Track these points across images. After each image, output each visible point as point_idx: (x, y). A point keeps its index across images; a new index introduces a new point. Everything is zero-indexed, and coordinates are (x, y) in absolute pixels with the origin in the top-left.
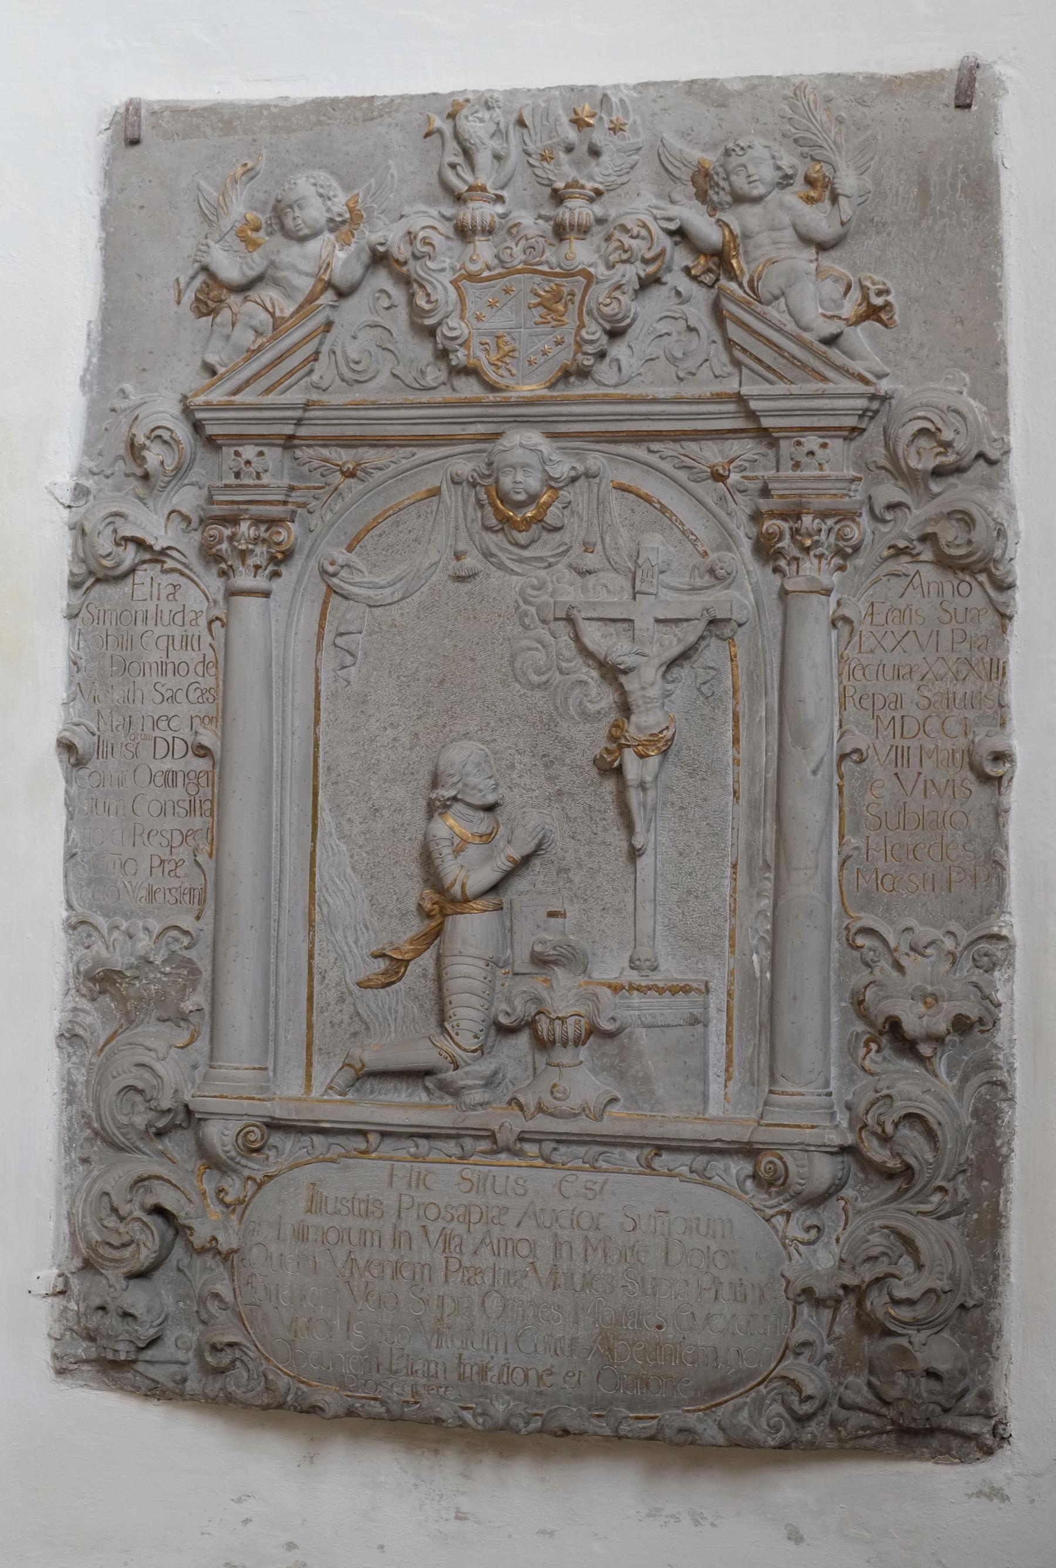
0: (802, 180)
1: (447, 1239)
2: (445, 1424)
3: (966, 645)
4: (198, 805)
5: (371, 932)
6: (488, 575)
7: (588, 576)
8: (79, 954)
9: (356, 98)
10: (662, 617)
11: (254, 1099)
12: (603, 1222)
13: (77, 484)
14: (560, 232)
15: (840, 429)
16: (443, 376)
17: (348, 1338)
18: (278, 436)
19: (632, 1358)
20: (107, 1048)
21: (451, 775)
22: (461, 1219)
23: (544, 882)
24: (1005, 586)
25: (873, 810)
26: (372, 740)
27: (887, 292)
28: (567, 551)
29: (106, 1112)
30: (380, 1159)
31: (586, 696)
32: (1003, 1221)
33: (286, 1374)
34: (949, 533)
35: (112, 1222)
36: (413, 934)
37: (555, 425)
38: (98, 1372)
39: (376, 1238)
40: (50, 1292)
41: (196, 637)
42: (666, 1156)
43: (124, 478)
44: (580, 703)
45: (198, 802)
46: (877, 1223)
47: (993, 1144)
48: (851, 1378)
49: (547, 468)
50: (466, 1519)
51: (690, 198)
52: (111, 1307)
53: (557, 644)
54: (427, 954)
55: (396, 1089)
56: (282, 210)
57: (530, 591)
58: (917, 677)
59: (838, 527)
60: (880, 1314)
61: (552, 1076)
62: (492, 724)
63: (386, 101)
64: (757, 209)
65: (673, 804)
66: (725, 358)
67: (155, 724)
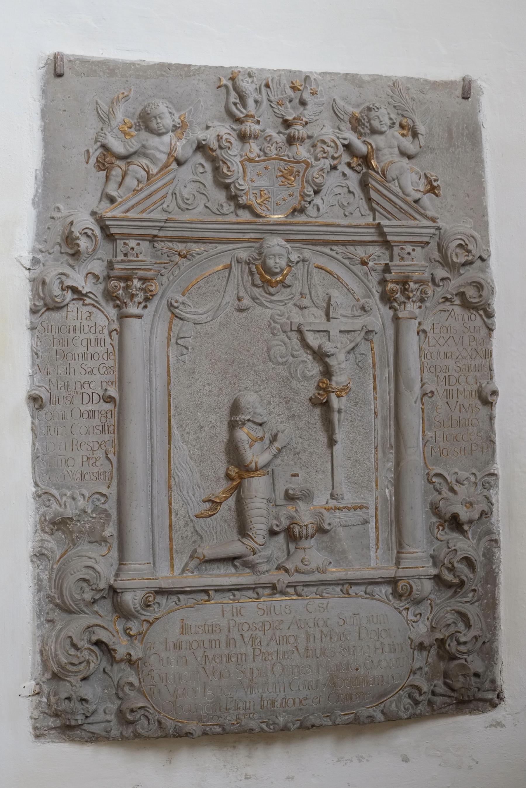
0: (398, 125)
1: (253, 639)
2: (254, 732)
3: (475, 343)
4: (106, 428)
5: (201, 489)
6: (254, 309)
7: (305, 310)
8: (43, 510)
9: (181, 65)
10: (343, 330)
11: (150, 579)
12: (329, 622)
13: (34, 257)
14: (291, 141)
15: (421, 242)
16: (232, 208)
17: (205, 696)
18: (149, 235)
19: (345, 686)
20: (62, 559)
21: (248, 408)
22: (260, 629)
23: (287, 460)
24: (490, 315)
25: (437, 419)
26: (198, 392)
27: (438, 180)
28: (293, 297)
29: (66, 593)
30: (216, 603)
31: (306, 368)
32: (497, 602)
33: (170, 719)
34: (471, 292)
35: (73, 652)
36: (223, 489)
37: (289, 235)
38: (59, 733)
39: (218, 643)
40: (32, 693)
41: (103, 340)
42: (354, 588)
43: (60, 255)
44: (303, 372)
45: (106, 426)
46: (448, 609)
47: (492, 567)
48: (436, 682)
49: (289, 256)
50: (250, 778)
51: (348, 129)
52: (74, 697)
53: (291, 343)
54: (230, 499)
55: (218, 567)
56: (150, 118)
57: (276, 317)
58: (454, 357)
59: (421, 288)
60: (454, 650)
61: (300, 554)
62: (259, 383)
63: (196, 68)
64: (382, 137)
65: (347, 419)
66: (366, 207)
67: (82, 386)
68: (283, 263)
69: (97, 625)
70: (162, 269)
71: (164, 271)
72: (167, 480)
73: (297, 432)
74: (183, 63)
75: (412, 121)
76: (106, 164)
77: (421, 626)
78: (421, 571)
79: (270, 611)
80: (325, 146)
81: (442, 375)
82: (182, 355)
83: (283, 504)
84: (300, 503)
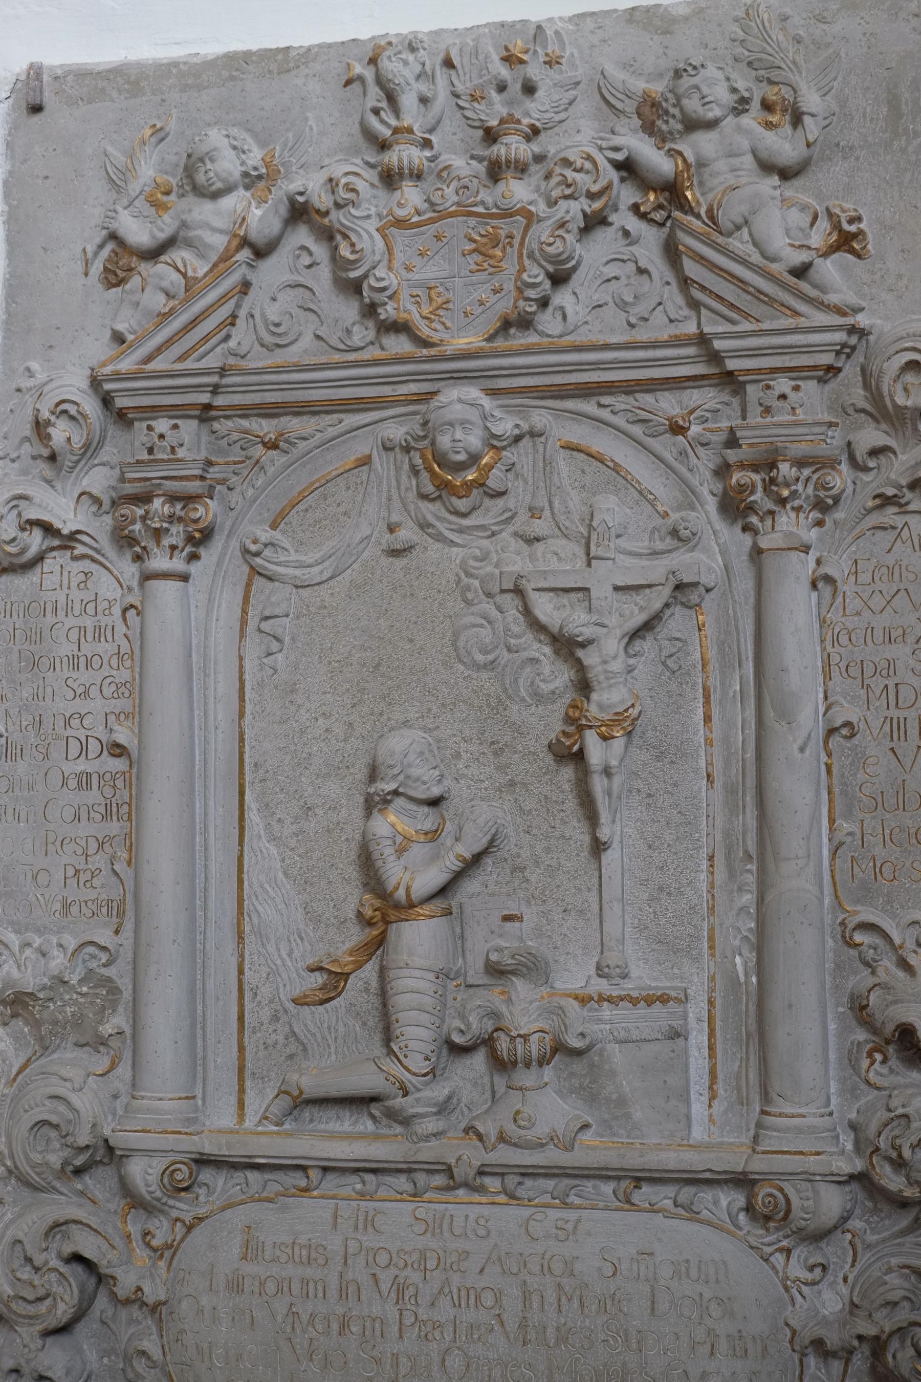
0: (759, 106)
1: (400, 1290)
4: (114, 809)
5: (306, 943)
6: (426, 548)
7: (537, 544)
9: (271, 50)
11: (179, 1133)
12: (578, 1267)
15: (815, 368)
16: (371, 334)
20: (20, 1077)
21: (391, 767)
22: (415, 1266)
25: (867, 790)
27: (859, 219)
28: (512, 518)
30: (322, 1197)
31: (538, 675)
36: (353, 944)
39: (320, 1288)
41: (110, 627)
42: (646, 1189)
44: (532, 683)
45: (114, 805)
46: (894, 1261)
49: (489, 425)
51: (634, 131)
54: (368, 966)
55: (338, 1117)
61: (514, 1101)
63: (301, 51)
65: (639, 791)
66: (680, 300)
67: (67, 723)
68: (474, 441)
69: (75, 1222)
70: (231, 475)
71: (234, 479)
72: (235, 921)
73: (519, 820)
74: (274, 46)
75: (793, 89)
76: (119, 272)
77: (828, 1295)
78: (812, 1163)
79: (441, 1226)
80: (570, 174)
81: (877, 685)
82: (269, 654)
83: (481, 982)
84: (518, 982)
